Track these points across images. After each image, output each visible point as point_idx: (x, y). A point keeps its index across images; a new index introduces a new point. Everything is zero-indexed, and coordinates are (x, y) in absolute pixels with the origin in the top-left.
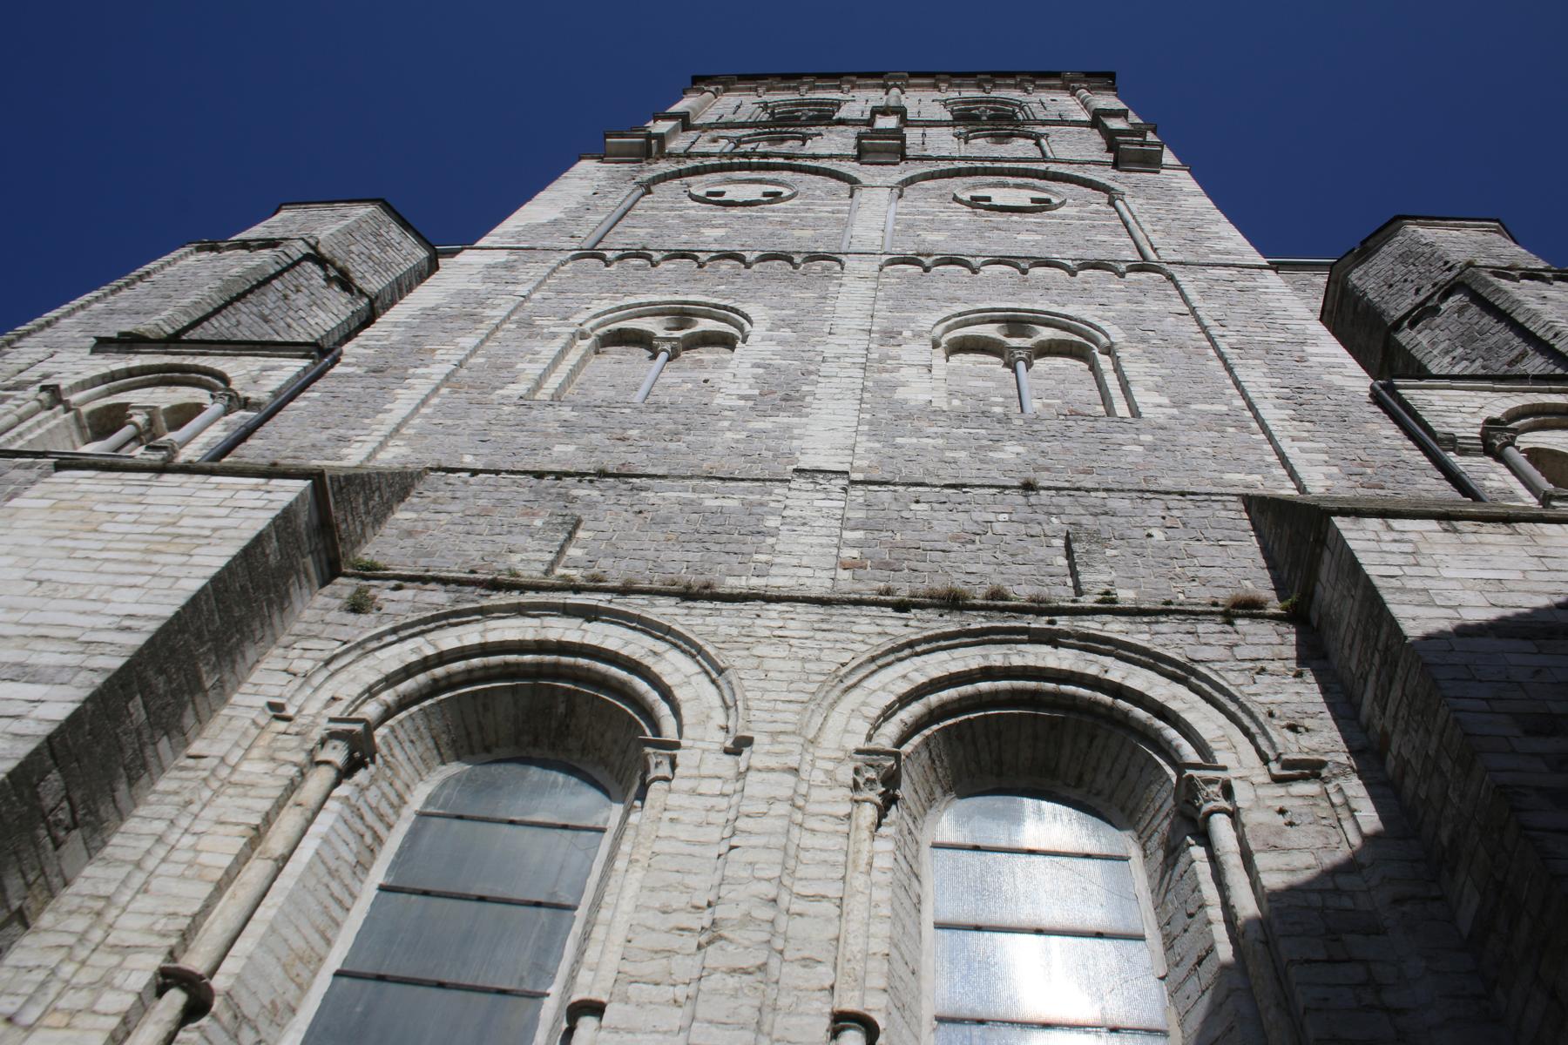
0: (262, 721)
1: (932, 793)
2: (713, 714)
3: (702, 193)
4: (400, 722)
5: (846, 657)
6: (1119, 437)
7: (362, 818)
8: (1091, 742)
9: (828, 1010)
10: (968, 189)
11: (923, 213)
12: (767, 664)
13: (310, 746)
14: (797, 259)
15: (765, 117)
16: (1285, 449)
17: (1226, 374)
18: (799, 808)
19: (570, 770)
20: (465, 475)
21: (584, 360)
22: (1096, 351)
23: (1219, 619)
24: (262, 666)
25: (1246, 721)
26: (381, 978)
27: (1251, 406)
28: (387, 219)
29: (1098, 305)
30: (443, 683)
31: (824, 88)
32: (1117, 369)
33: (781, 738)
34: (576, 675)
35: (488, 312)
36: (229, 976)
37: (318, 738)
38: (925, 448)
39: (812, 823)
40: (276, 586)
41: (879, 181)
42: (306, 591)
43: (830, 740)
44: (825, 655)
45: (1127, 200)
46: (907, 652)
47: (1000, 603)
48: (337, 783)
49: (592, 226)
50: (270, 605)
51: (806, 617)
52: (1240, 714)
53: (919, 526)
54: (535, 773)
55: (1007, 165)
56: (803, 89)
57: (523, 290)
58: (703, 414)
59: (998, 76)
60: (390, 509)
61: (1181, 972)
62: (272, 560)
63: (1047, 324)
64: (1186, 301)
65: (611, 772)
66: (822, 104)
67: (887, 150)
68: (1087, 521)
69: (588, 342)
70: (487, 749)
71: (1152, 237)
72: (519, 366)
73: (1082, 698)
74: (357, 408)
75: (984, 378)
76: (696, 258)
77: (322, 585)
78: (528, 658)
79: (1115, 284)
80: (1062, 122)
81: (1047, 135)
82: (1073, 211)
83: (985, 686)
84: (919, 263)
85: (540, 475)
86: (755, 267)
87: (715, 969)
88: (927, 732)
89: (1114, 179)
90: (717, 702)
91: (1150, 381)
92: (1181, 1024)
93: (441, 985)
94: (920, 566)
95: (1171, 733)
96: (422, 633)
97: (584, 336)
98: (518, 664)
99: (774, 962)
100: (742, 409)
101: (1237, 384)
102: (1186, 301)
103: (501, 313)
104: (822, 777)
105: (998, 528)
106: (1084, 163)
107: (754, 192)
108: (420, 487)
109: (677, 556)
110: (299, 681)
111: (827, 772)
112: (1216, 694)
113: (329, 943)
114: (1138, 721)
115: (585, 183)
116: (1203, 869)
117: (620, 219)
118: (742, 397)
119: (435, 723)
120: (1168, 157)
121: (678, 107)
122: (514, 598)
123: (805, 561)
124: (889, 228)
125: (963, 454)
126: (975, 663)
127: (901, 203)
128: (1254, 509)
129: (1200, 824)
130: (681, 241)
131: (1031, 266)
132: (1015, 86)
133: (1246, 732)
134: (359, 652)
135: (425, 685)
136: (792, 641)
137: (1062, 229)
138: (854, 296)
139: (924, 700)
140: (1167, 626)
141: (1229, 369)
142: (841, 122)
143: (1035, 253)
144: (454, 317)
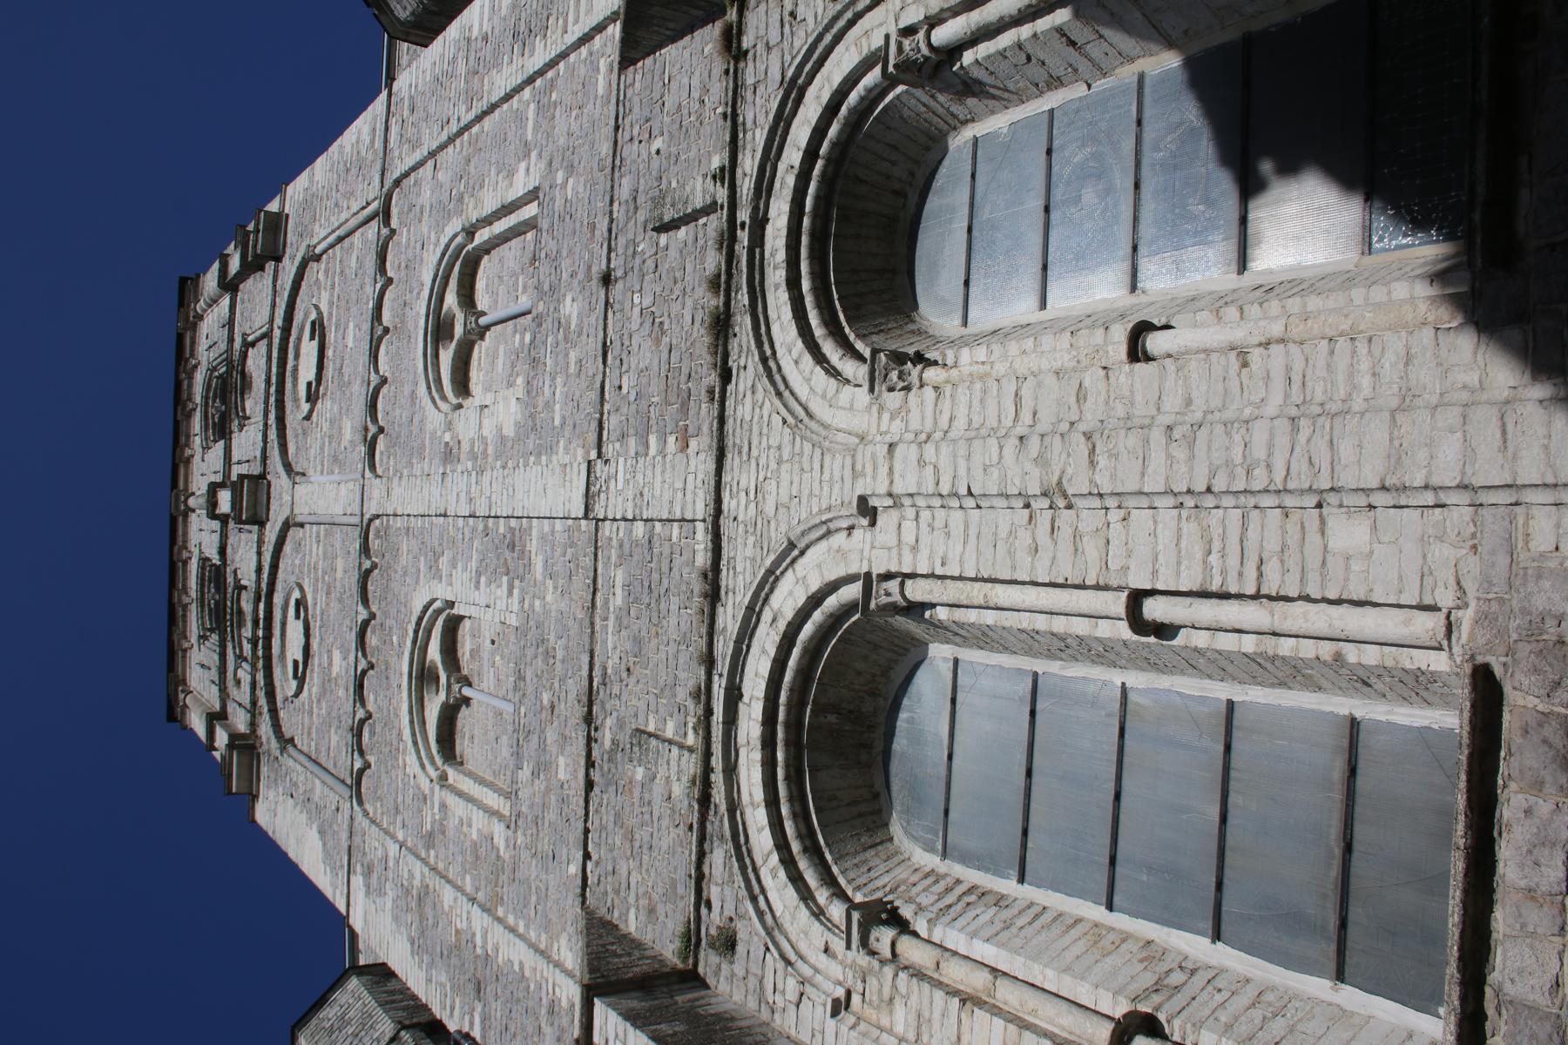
0: (851, 1020)
1: (913, 332)
2: (835, 547)
3: (294, 684)
4: (849, 882)
5: (777, 420)
6: (559, 203)
7: (950, 906)
8: (862, 181)
9: (1127, 367)
10: (298, 407)
11: (322, 449)
12: (784, 498)
13: (876, 964)
14: (367, 564)
15: (215, 637)
16: (575, 38)
17: (497, 112)
18: (929, 437)
19: (896, 707)
20: (590, 865)
21: (470, 774)
22: (470, 247)
23: (742, 65)
24: (793, 1032)
25: (841, 23)
26: (1113, 861)
27: (530, 80)
28: (314, 1021)
29: (422, 249)
30: (808, 843)
31: (185, 579)
32: (488, 221)
33: (859, 467)
34: (797, 705)
35: (417, 882)
36: (1115, 1003)
37: (868, 958)
38: (564, 395)
39: (944, 422)
40: (707, 1024)
41: (287, 498)
42: (713, 1000)
43: (860, 422)
44: (774, 442)
45: (315, 241)
46: (772, 364)
47: (723, 278)
48: (915, 934)
49: (327, 791)
50: (729, 1029)
51: (736, 470)
52: (834, 31)
53: (644, 380)
54: (900, 744)
55: (274, 370)
56: (186, 600)
57: (393, 849)
58: (529, 635)
59: (179, 398)
60: (625, 936)
61: (1083, 65)
62: (680, 1028)
63: (441, 300)
64: (420, 164)
65: (896, 662)
66: (203, 579)
67: (254, 494)
68: (641, 216)
69: (451, 772)
70: (876, 796)
71: (355, 208)
72: (475, 836)
73: (819, 189)
74: (518, 1000)
75: (495, 357)
76: (364, 672)
77: (707, 987)
78: (780, 756)
79: (403, 237)
80: (230, 323)
81: (245, 335)
82: (325, 296)
83: (806, 285)
84: (375, 438)
85: (589, 785)
86: (374, 609)
87: (1091, 481)
88: (852, 337)
89: (293, 258)
90: (823, 544)
91: (503, 184)
92: (1132, 60)
93: (1117, 797)
94: (685, 371)
95: (853, 98)
96: (755, 870)
97: (443, 777)
98: (787, 766)
99: (1082, 427)
100: (522, 590)
101: (508, 97)
102: (420, 164)
103: (418, 867)
104: (898, 422)
105: (647, 301)
106: (275, 291)
107: (295, 629)
108: (602, 912)
109: (673, 621)
110: (808, 989)
111: (892, 418)
112: (815, 56)
113: (1078, 921)
114: (841, 132)
115: (280, 810)
116: (984, 49)
117: (320, 765)
118: (510, 593)
119: (850, 848)
120: (273, 207)
121: (200, 729)
122: (717, 778)
123: (679, 485)
124: (336, 477)
125: (573, 356)
126: (784, 296)
127: (311, 472)
128: (633, 55)
129: (943, 57)
130: (344, 694)
131: (380, 323)
132: (191, 378)
133: (851, 23)
134: (776, 933)
135: (811, 860)
136: (761, 478)
137: (343, 303)
138: (407, 494)
139: (820, 341)
140: (748, 114)
141: (493, 107)
142: (222, 551)
143: (366, 326)
144: (422, 917)
